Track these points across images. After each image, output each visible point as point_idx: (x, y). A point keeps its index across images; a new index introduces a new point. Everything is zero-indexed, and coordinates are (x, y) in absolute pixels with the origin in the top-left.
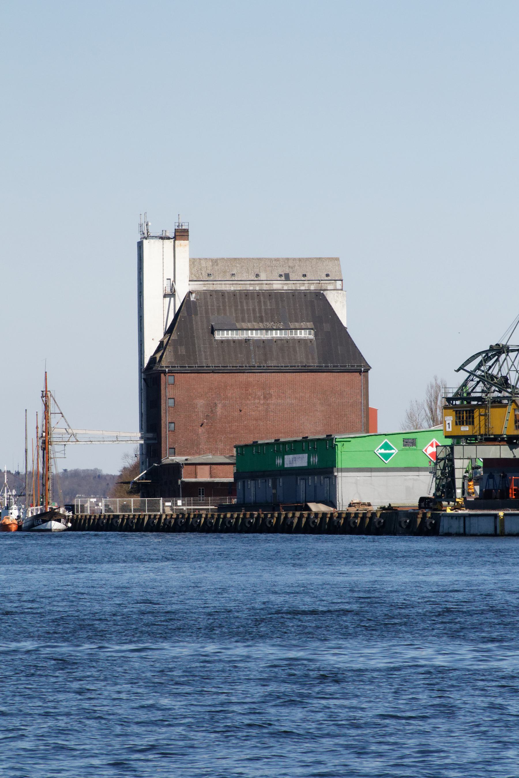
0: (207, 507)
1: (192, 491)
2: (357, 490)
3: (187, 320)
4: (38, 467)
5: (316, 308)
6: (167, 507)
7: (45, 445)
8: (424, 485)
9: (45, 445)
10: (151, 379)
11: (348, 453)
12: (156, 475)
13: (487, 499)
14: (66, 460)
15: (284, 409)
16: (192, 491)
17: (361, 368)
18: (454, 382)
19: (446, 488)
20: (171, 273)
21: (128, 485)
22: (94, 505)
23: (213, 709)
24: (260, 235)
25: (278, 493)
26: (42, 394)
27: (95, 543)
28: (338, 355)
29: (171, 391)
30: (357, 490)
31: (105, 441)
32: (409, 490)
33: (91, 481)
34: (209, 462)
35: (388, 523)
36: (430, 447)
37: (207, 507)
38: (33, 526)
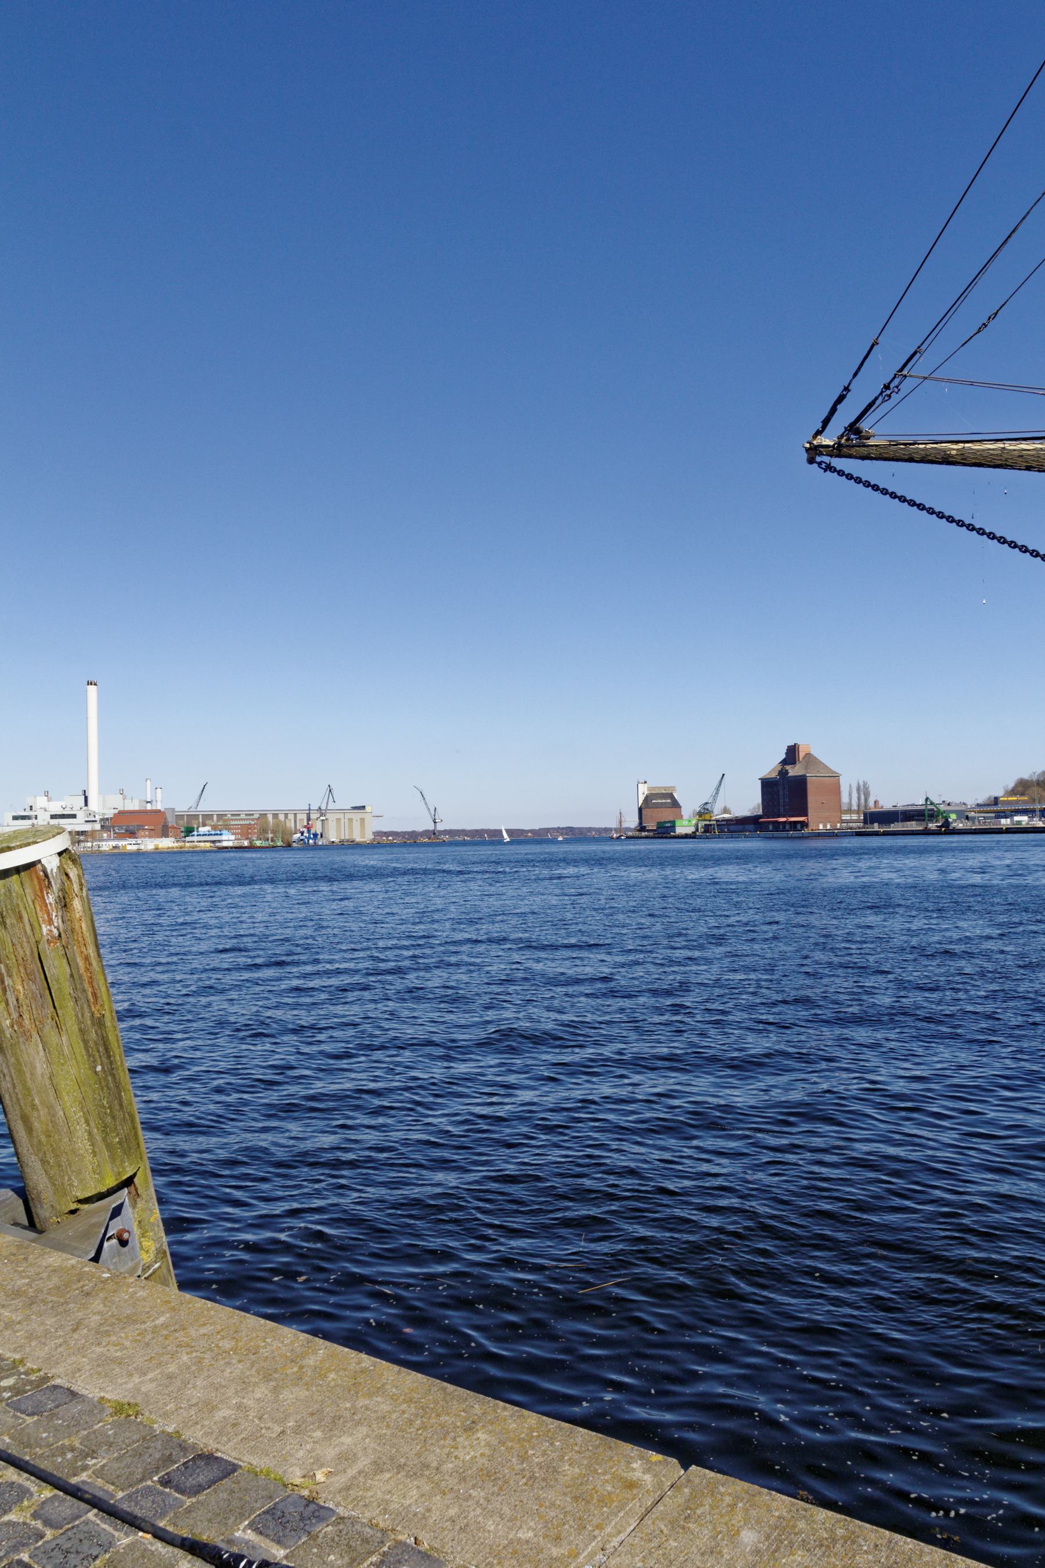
0: (651, 834)
1: (648, 831)
2: (680, 830)
3: (647, 799)
4: (851, 800)
5: (671, 796)
6: (644, 834)
7: (621, 822)
8: (693, 829)
9: (621, 822)
10: (640, 810)
11: (678, 823)
12: (642, 828)
13: (705, 832)
14: (625, 825)
15: (665, 815)
16: (648, 831)
17: (680, 807)
18: (698, 809)
19: (697, 830)
20: (644, 790)
21: (636, 830)
22: (630, 834)
23: (1027, 1277)
24: (660, 781)
25: (665, 831)
26: (900, 383)
27: (632, 841)
28: (675, 804)
29: (644, 812)
30: (680, 830)
31: (632, 821)
32: (690, 830)
33: (629, 829)
34: (651, 825)
35: (686, 836)
36: (694, 822)
37: (651, 834)
38: (618, 838)
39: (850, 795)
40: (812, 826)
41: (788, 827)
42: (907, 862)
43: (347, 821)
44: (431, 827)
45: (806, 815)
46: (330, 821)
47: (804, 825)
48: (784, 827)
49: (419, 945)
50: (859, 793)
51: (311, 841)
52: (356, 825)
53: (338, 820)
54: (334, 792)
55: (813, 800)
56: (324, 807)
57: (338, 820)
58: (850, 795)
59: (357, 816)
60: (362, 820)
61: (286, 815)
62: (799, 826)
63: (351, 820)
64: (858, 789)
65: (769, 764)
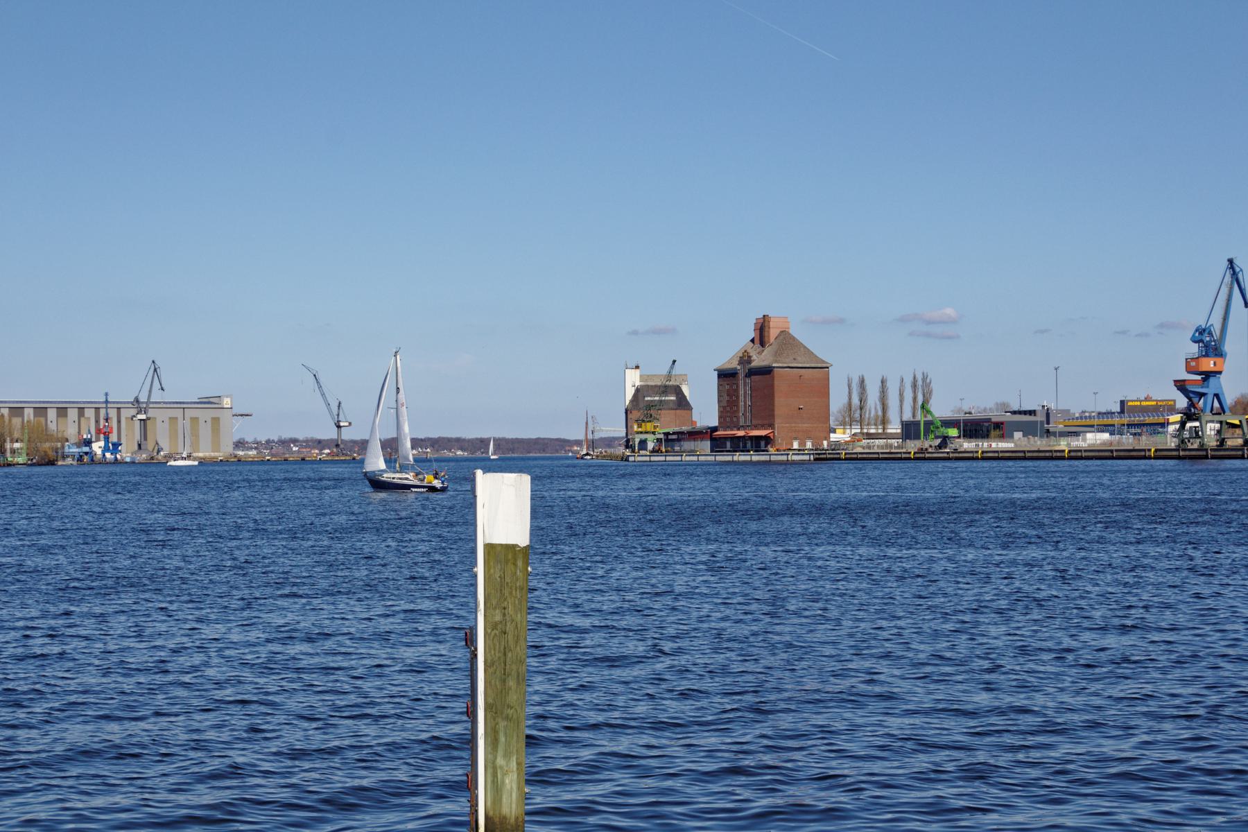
5: (678, 391)
20: (633, 379)
39: (901, 395)
40: (780, 442)
41: (749, 444)
42: (674, 494)
43: (187, 422)
44: (330, 433)
45: (771, 426)
46: (159, 421)
47: (768, 440)
48: (745, 446)
49: (1002, 713)
50: (915, 392)
51: (108, 455)
52: (205, 431)
53: (173, 420)
54: (162, 372)
55: (782, 404)
56: (143, 399)
57: (173, 420)
58: (901, 395)
59: (205, 415)
60: (216, 421)
61: (81, 411)
62: (763, 443)
63: (195, 420)
64: (914, 386)
65: (730, 344)
